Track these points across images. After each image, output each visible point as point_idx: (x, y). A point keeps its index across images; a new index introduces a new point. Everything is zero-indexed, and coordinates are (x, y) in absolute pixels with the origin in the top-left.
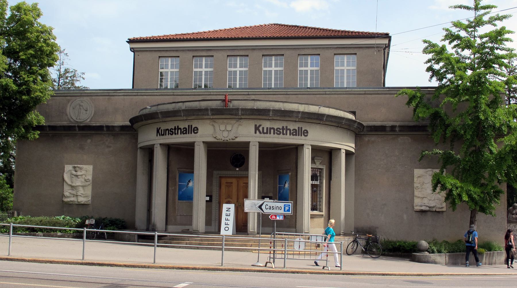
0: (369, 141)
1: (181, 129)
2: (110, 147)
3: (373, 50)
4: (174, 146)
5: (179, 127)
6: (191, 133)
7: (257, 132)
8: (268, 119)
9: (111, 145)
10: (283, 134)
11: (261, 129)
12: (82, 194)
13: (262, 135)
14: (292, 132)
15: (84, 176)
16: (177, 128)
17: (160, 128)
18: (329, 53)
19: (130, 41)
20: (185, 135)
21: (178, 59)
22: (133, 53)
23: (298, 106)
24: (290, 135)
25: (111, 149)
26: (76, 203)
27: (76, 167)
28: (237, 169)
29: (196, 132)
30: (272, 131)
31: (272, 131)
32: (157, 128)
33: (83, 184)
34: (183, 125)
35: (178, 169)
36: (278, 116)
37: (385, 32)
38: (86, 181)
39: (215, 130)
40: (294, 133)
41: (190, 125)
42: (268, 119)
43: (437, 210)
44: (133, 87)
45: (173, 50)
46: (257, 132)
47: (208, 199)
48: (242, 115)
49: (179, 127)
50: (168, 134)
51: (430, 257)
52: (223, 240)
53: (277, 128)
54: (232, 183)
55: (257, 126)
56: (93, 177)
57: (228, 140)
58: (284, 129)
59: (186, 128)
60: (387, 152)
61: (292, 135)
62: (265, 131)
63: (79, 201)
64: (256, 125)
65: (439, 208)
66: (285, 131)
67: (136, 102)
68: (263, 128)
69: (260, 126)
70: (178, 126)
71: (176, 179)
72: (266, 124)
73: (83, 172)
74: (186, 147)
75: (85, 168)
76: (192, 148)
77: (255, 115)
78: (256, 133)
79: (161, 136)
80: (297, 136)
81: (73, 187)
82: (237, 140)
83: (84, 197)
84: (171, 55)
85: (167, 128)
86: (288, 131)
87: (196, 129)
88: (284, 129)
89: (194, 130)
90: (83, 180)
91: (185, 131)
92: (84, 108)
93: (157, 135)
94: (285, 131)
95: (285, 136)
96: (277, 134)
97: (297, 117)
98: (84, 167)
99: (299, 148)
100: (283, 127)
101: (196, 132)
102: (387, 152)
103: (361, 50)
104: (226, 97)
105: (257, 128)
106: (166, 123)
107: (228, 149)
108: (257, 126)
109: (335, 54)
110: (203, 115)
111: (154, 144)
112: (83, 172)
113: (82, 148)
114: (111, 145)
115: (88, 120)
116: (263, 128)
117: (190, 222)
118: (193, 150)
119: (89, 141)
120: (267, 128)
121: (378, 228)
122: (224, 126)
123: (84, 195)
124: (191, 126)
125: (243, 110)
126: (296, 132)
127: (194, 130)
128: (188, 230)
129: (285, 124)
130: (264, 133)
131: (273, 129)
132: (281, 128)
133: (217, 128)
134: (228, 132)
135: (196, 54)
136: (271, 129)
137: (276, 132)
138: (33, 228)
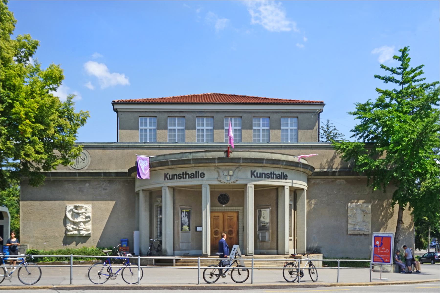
0: (314, 183)
1: (188, 174)
2: (106, 189)
3: (311, 114)
4: (177, 188)
5: (187, 173)
6: (198, 177)
7: (253, 176)
8: (261, 166)
9: (107, 188)
10: (183, 178)
11: (255, 174)
12: (83, 228)
13: (257, 178)
14: (190, 175)
15: (84, 214)
16: (184, 173)
17: (168, 174)
18: (275, 117)
19: (114, 103)
20: (193, 179)
21: (156, 119)
22: (115, 113)
23: (268, 155)
24: (189, 178)
25: (107, 191)
26: (79, 235)
27: (77, 206)
28: (224, 206)
29: (202, 176)
30: (264, 175)
31: (264, 175)
32: (165, 174)
33: (84, 220)
34: (190, 171)
35: (180, 206)
36: (269, 164)
37: (321, 100)
38: (87, 217)
39: (219, 175)
40: (192, 177)
41: (197, 171)
42: (261, 166)
43: (365, 233)
44: (117, 141)
45: (151, 112)
46: (253, 176)
47: (199, 229)
48: (243, 162)
49: (187, 173)
50: (177, 179)
51: (385, 268)
52: (198, 261)
53: (267, 173)
54: (218, 216)
55: (253, 171)
56: (92, 214)
57: (230, 182)
58: (184, 174)
59: (194, 174)
60: (328, 191)
61: (190, 179)
62: (259, 176)
63: (81, 234)
64: (251, 171)
65: (367, 232)
66: (272, 176)
67: (128, 153)
68: (257, 173)
69: (255, 171)
70: (186, 172)
71: (179, 214)
72: (260, 171)
73: (83, 211)
74: (185, 189)
75: (85, 207)
76: (200, 190)
77: (253, 163)
78: (252, 177)
79: (169, 180)
80: (195, 179)
81: (74, 223)
82: (238, 183)
83: (86, 231)
84: (290, 116)
85: (175, 174)
86: (187, 176)
87: (202, 174)
88: (184, 174)
89: (201, 175)
90: (84, 217)
91: (192, 176)
92: (81, 158)
93: (165, 180)
94: (272, 176)
95: (185, 179)
96: (179, 178)
97: (282, 164)
98: (85, 206)
99: (280, 190)
100: (183, 173)
101: (202, 176)
102: (328, 191)
103: (302, 114)
104: (228, 149)
105: (252, 173)
106: (174, 170)
107: (215, 190)
108: (253, 171)
109: (140, 117)
110: (211, 163)
111: (162, 187)
112: (83, 211)
113: (81, 191)
114: (107, 188)
115: (86, 168)
116: (257, 173)
117: (200, 248)
118: (200, 192)
119: (87, 185)
120: (260, 173)
121: (321, 247)
122: (227, 172)
123: (85, 229)
124: (198, 172)
125: (267, 159)
126: (280, 176)
127: (201, 175)
128: (189, 254)
129: (272, 170)
130: (258, 177)
131: (264, 173)
132: (270, 173)
133: (221, 174)
134: (230, 177)
135: (227, 115)
136: (263, 174)
137: (178, 177)
138: (77, 257)
